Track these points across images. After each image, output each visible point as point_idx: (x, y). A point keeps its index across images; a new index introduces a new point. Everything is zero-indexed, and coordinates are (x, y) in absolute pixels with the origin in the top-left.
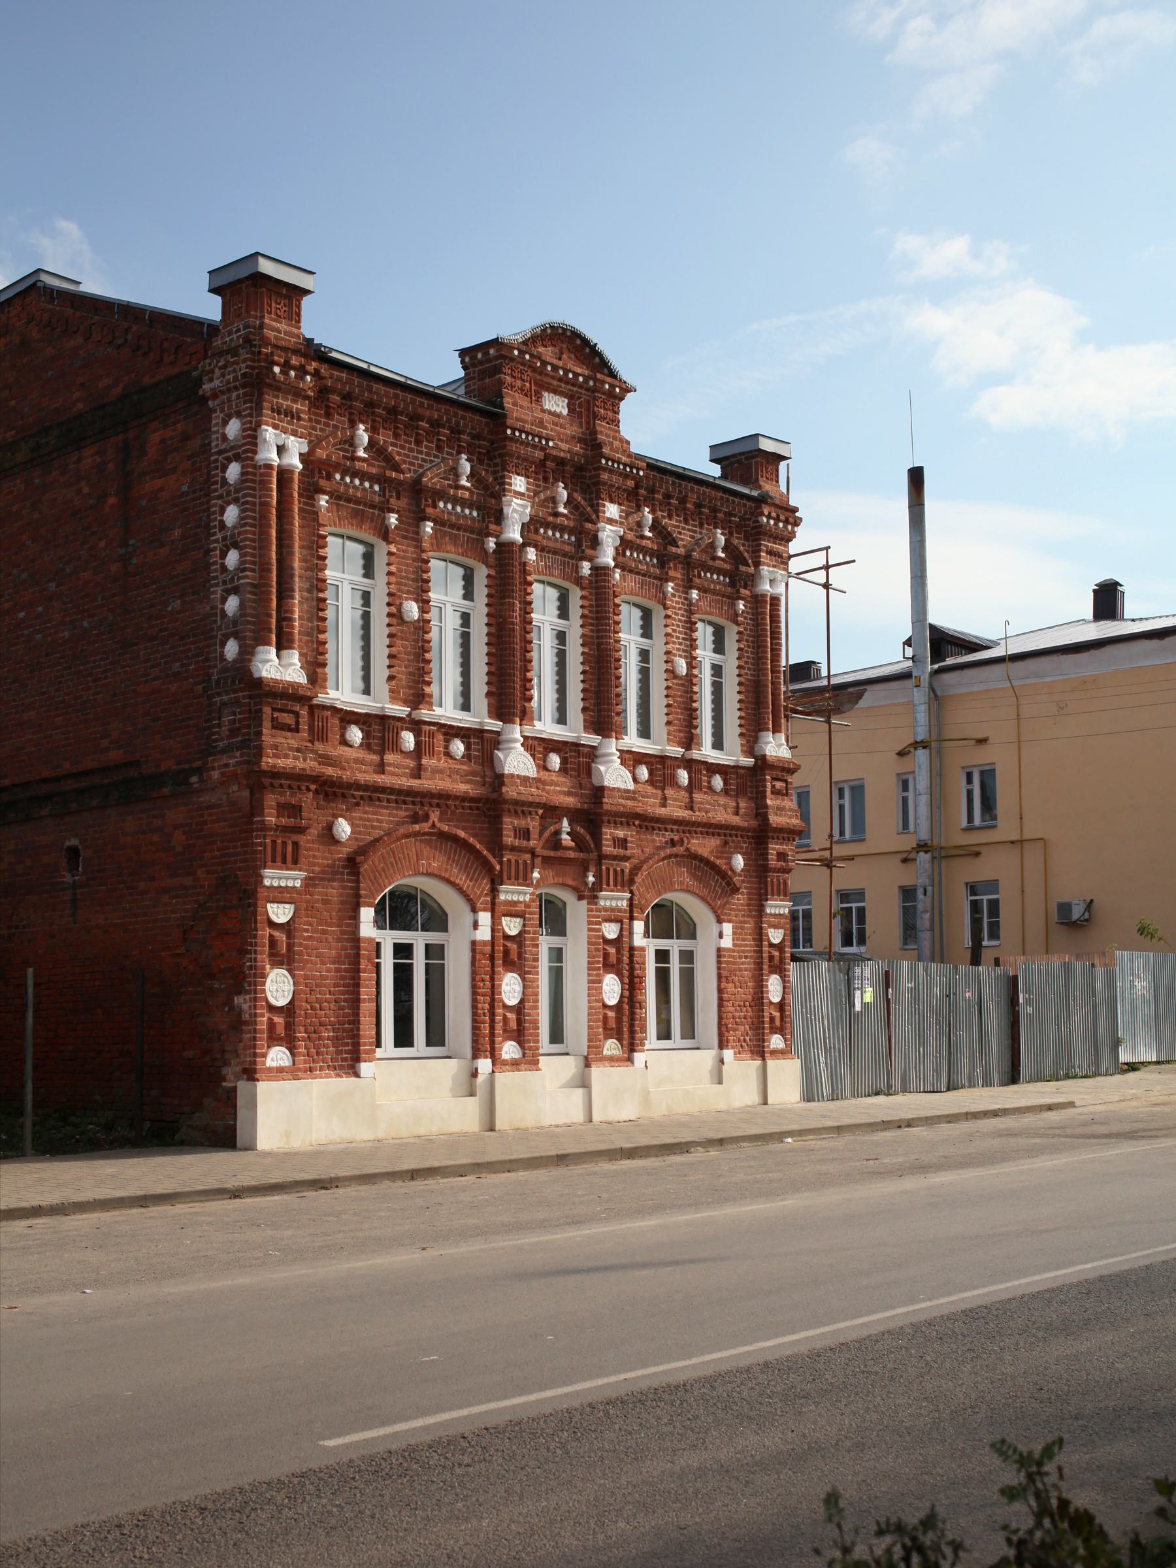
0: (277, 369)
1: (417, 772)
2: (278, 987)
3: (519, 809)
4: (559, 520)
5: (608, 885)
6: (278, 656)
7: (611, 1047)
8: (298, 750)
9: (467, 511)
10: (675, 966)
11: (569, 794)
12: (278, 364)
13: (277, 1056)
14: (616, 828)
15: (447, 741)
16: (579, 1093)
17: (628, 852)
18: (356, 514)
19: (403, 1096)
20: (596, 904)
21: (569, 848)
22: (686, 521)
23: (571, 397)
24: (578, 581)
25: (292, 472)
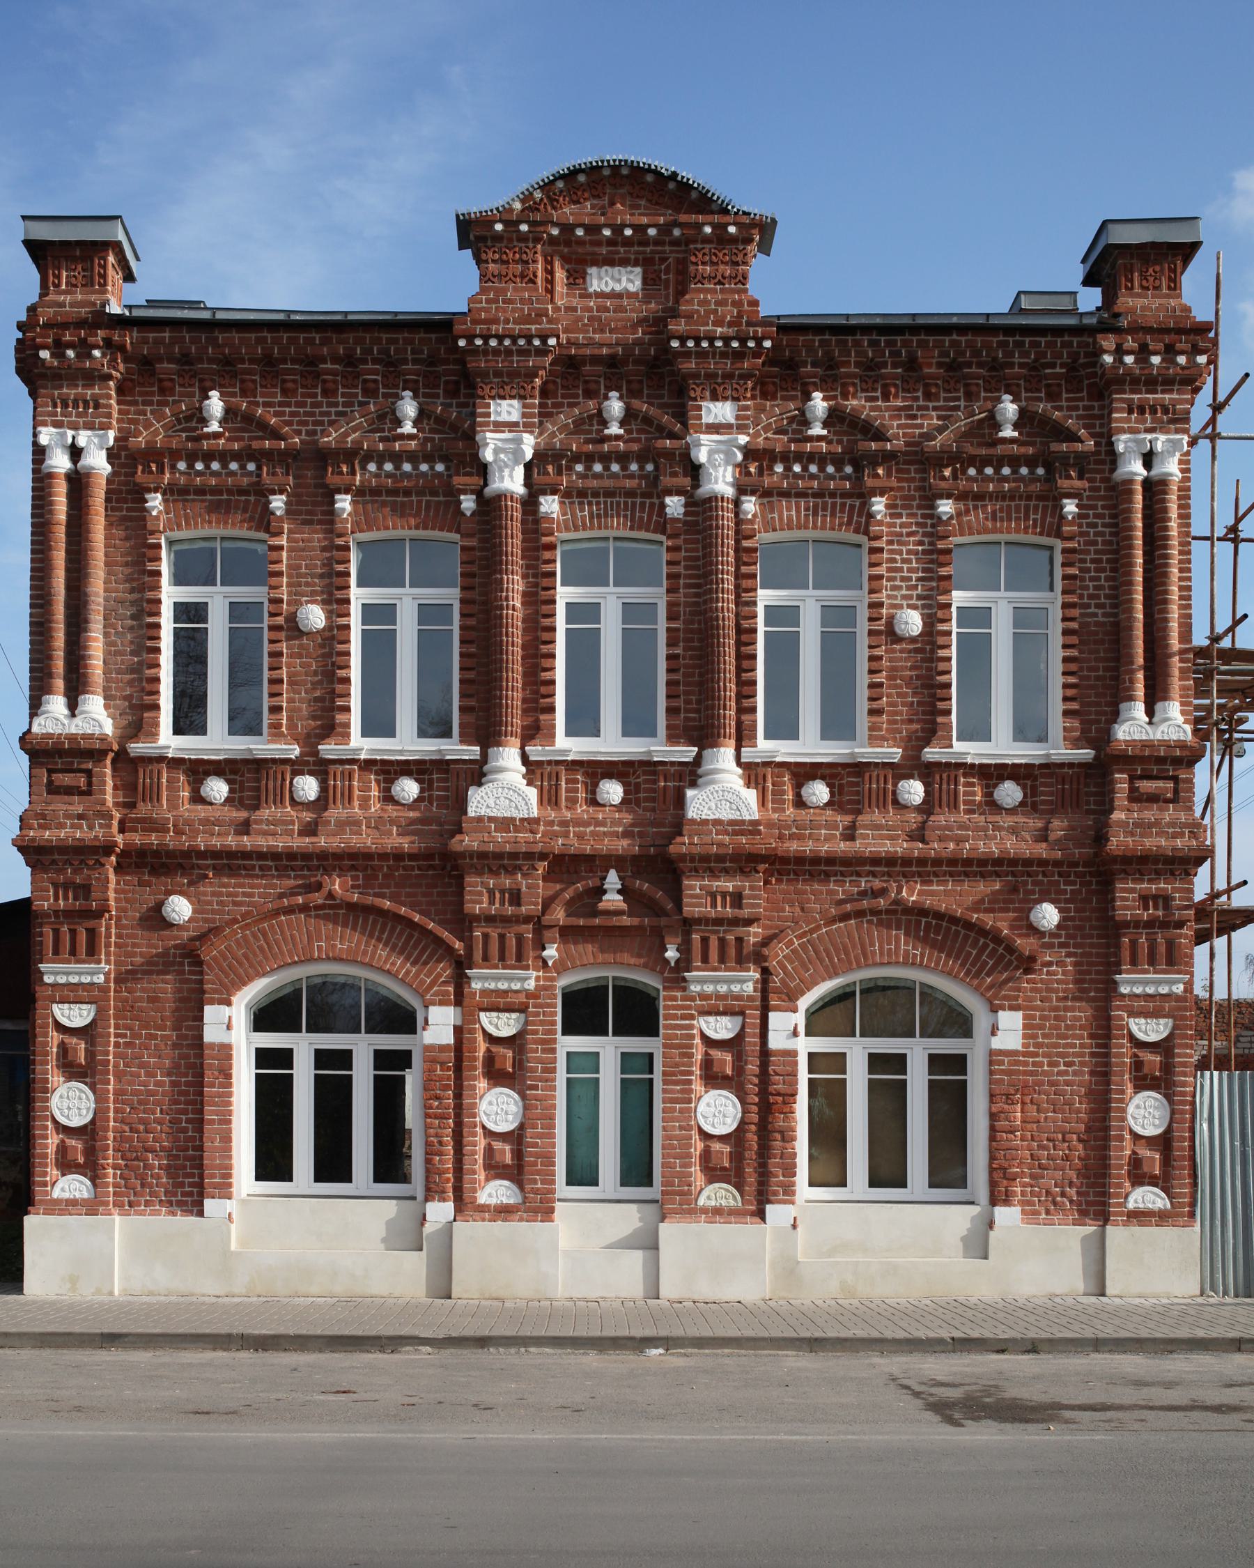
0: (45, 354)
1: (310, 830)
2: (69, 1103)
4: (1000, 449)
5: (705, 959)
6: (1150, 712)
8: (80, 817)
9: (424, 467)
10: (918, 1081)
11: (626, 834)
12: (44, 347)
13: (73, 1186)
16: (636, 1258)
17: (745, 913)
18: (214, 508)
19: (286, 1240)
20: (684, 989)
21: (619, 913)
22: (928, 396)
23: (646, 263)
24: (662, 524)
25: (1131, 482)
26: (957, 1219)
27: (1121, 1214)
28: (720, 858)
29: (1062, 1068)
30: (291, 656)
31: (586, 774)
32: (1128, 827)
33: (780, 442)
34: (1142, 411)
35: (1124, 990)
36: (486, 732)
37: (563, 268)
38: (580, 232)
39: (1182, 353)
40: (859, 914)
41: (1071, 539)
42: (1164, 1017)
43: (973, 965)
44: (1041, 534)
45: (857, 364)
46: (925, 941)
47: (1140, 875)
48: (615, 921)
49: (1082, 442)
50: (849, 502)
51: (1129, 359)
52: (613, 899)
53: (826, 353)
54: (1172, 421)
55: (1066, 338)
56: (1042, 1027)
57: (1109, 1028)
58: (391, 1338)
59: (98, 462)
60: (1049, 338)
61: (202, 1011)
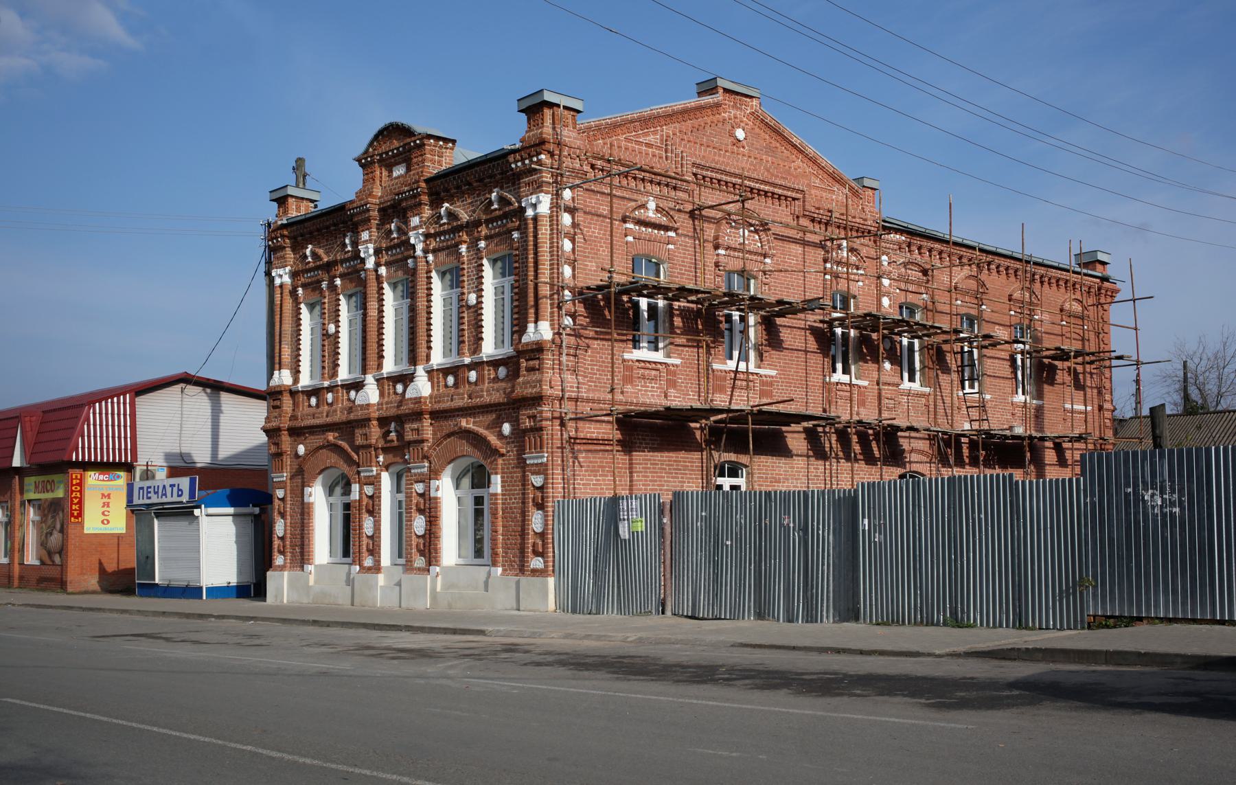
7: (420, 562)
15: (348, 393)
52: (393, 434)
59: (287, 279)
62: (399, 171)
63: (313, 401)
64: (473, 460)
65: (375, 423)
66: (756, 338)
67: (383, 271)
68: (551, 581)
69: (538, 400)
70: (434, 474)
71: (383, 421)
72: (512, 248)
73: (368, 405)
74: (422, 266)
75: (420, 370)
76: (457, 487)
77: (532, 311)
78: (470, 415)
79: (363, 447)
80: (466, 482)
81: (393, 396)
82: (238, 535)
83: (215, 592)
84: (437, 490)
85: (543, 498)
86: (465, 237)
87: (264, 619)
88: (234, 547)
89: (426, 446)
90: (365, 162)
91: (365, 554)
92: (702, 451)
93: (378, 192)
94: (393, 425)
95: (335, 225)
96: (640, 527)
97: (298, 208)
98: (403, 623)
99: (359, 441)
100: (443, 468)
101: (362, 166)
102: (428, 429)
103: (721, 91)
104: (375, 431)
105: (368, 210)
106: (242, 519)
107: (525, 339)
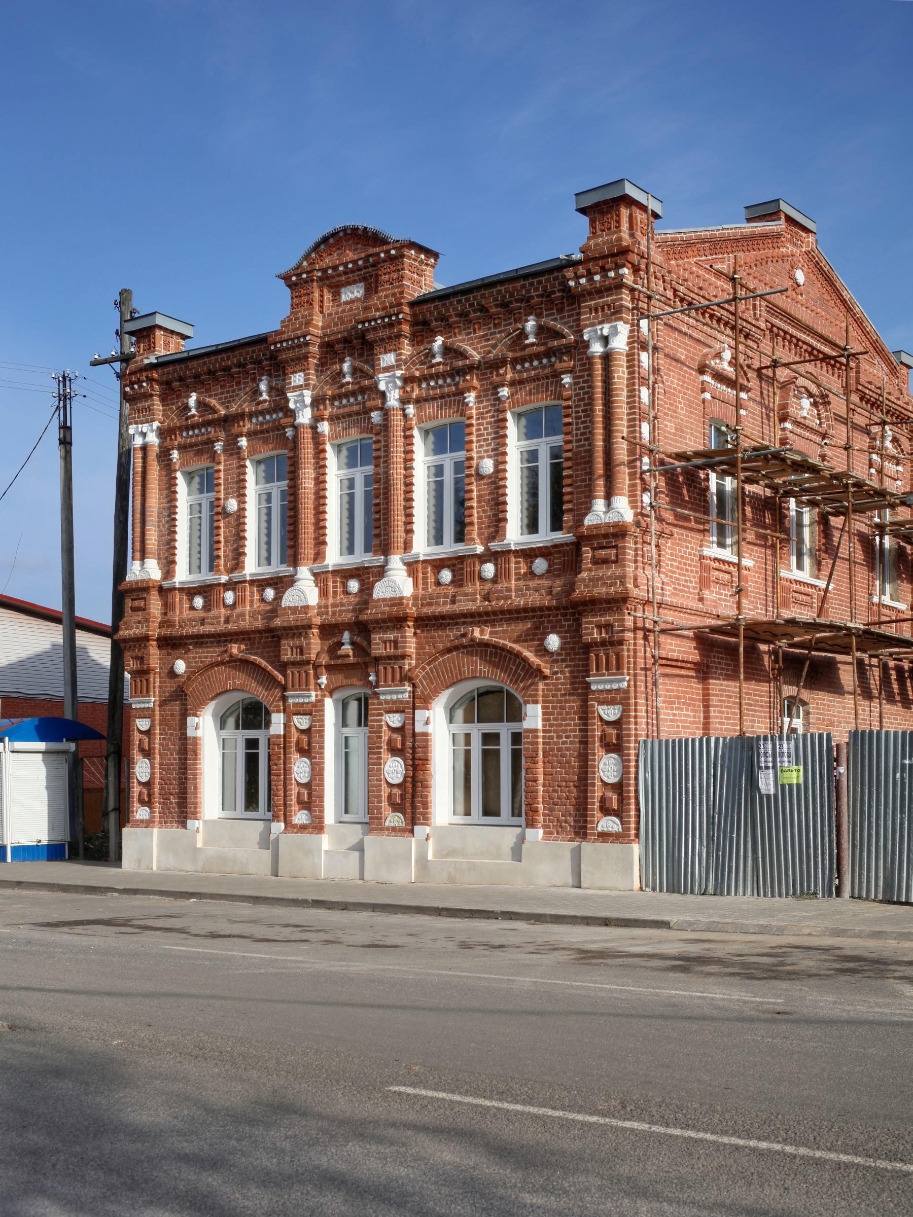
2: (142, 769)
3: (291, 632)
7: (394, 819)
8: (139, 622)
14: (385, 632)
15: (191, 600)
20: (378, 698)
26: (509, 836)
27: (594, 834)
28: (384, 621)
29: (564, 739)
30: (225, 527)
31: (341, 577)
32: (589, 581)
33: (177, 422)
34: (596, 310)
35: (593, 687)
36: (385, 549)
37: (329, 292)
38: (330, 272)
39: (610, 270)
40: (456, 648)
41: (569, 399)
42: (617, 704)
43: (514, 676)
44: (554, 399)
45: (456, 315)
46: (490, 662)
47: (594, 613)
48: (347, 661)
49: (565, 338)
50: (457, 398)
51: (583, 281)
52: (347, 649)
53: (439, 313)
54: (613, 314)
55: (556, 274)
56: (552, 714)
57: (586, 713)
58: (105, 888)
59: (153, 439)
60: (547, 277)
61: (186, 720)
62: (353, 293)
63: (199, 602)
64: (237, 697)
65: (315, 631)
66: (812, 541)
67: (325, 427)
68: (636, 849)
69: (619, 602)
70: (420, 700)
71: (329, 630)
72: (560, 397)
73: (402, 598)
74: (397, 421)
75: (304, 573)
76: (222, 725)
77: (601, 482)
78: (485, 623)
79: (294, 664)
80: (460, 714)
81: (340, 597)
82: (49, 779)
83: (25, 853)
84: (427, 723)
85: (619, 737)
86: (475, 382)
87: (213, 896)
88: (45, 794)
89: (407, 664)
90: (296, 282)
91: (294, 807)
92: (769, 682)
93: (318, 320)
94: (346, 636)
95: (240, 365)
96: (794, 776)
97: (167, 345)
98: (498, 908)
99: (287, 655)
100: (436, 692)
101: (292, 286)
102: (410, 640)
103: (783, 217)
104: (315, 645)
105: (307, 344)
106: (54, 757)
107: (589, 520)
